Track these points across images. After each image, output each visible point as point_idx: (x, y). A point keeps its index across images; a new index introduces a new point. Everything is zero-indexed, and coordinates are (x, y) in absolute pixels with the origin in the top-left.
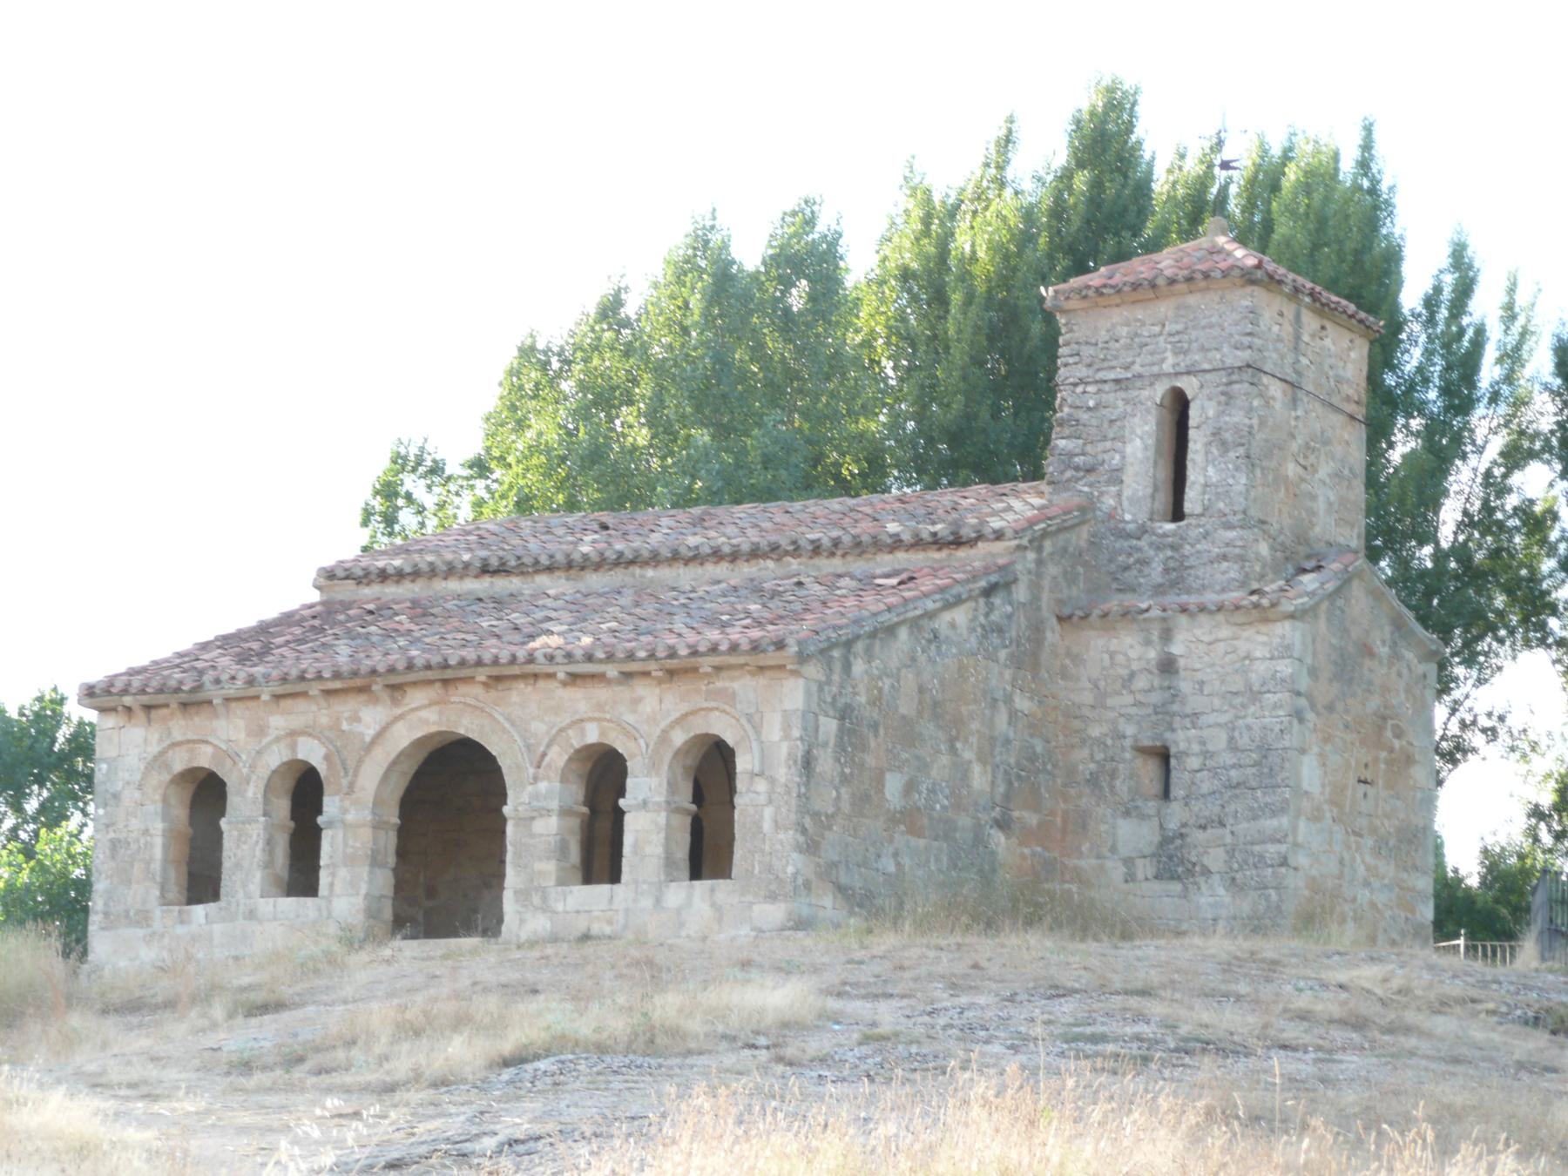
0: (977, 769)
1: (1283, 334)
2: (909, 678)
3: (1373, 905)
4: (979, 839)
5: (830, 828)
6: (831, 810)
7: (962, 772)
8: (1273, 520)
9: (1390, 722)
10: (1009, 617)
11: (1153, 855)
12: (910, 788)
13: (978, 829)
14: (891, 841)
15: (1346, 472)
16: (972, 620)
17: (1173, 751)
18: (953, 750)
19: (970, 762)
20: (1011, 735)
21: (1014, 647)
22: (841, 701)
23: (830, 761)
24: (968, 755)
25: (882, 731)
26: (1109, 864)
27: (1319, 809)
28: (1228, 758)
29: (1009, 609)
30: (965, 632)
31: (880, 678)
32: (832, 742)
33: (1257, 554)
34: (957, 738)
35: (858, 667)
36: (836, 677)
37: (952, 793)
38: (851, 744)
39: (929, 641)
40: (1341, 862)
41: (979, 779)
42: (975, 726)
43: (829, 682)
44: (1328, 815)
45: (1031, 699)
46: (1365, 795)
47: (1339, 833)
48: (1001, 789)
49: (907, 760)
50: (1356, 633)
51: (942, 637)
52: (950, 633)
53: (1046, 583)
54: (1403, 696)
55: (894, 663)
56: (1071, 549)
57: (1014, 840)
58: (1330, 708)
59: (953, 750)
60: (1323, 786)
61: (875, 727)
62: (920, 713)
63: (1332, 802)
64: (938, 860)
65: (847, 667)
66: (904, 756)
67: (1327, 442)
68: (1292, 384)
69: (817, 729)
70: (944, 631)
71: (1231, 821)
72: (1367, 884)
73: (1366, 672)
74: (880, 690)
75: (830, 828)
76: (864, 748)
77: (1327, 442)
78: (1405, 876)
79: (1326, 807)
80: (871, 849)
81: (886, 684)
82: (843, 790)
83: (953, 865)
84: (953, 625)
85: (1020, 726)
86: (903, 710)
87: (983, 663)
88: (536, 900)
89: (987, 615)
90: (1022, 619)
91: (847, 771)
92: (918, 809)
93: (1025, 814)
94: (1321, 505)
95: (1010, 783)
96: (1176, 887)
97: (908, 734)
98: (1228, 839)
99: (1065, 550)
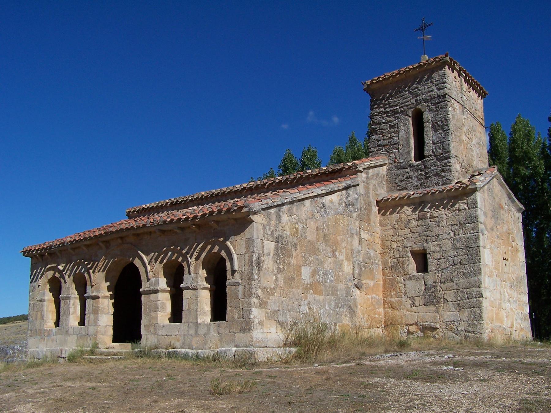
0: (346, 263)
1: (457, 85)
2: (312, 224)
4: (348, 293)
5: (273, 294)
6: (273, 286)
7: (339, 265)
8: (460, 156)
10: (357, 199)
12: (314, 273)
13: (348, 289)
14: (306, 298)
15: (481, 143)
16: (340, 200)
17: (428, 251)
18: (334, 255)
19: (343, 261)
20: (360, 249)
21: (359, 212)
22: (276, 234)
23: (271, 262)
24: (341, 257)
25: (298, 248)
26: (404, 300)
27: (492, 272)
28: (453, 253)
29: (356, 196)
30: (337, 205)
31: (297, 223)
32: (272, 254)
33: (456, 169)
34: (336, 250)
35: (285, 218)
36: (273, 222)
37: (335, 275)
38: (282, 254)
39: (321, 208)
41: (347, 268)
42: (344, 245)
43: (269, 225)
44: (495, 274)
45: (368, 234)
48: (357, 272)
49: (312, 261)
51: (327, 207)
52: (330, 205)
53: (371, 187)
55: (304, 216)
56: (380, 175)
57: (364, 292)
58: (492, 229)
59: (334, 255)
61: (295, 246)
62: (318, 240)
63: (496, 269)
64: (330, 305)
65: (279, 218)
66: (311, 259)
67: (474, 131)
69: (263, 247)
70: (327, 204)
71: (456, 279)
73: (502, 216)
74: (297, 229)
75: (273, 294)
76: (290, 256)
77: (474, 131)
78: (520, 296)
79: (494, 271)
80: (296, 303)
81: (300, 226)
82: (279, 276)
83: (337, 306)
84: (332, 202)
85: (363, 245)
86: (309, 238)
87: (346, 218)
88: (152, 330)
89: (347, 198)
90: (362, 201)
91: (281, 267)
92: (319, 282)
93: (368, 281)
94: (475, 154)
95: (361, 269)
96: (433, 308)
97: (312, 249)
98: (455, 287)
99: (378, 174)
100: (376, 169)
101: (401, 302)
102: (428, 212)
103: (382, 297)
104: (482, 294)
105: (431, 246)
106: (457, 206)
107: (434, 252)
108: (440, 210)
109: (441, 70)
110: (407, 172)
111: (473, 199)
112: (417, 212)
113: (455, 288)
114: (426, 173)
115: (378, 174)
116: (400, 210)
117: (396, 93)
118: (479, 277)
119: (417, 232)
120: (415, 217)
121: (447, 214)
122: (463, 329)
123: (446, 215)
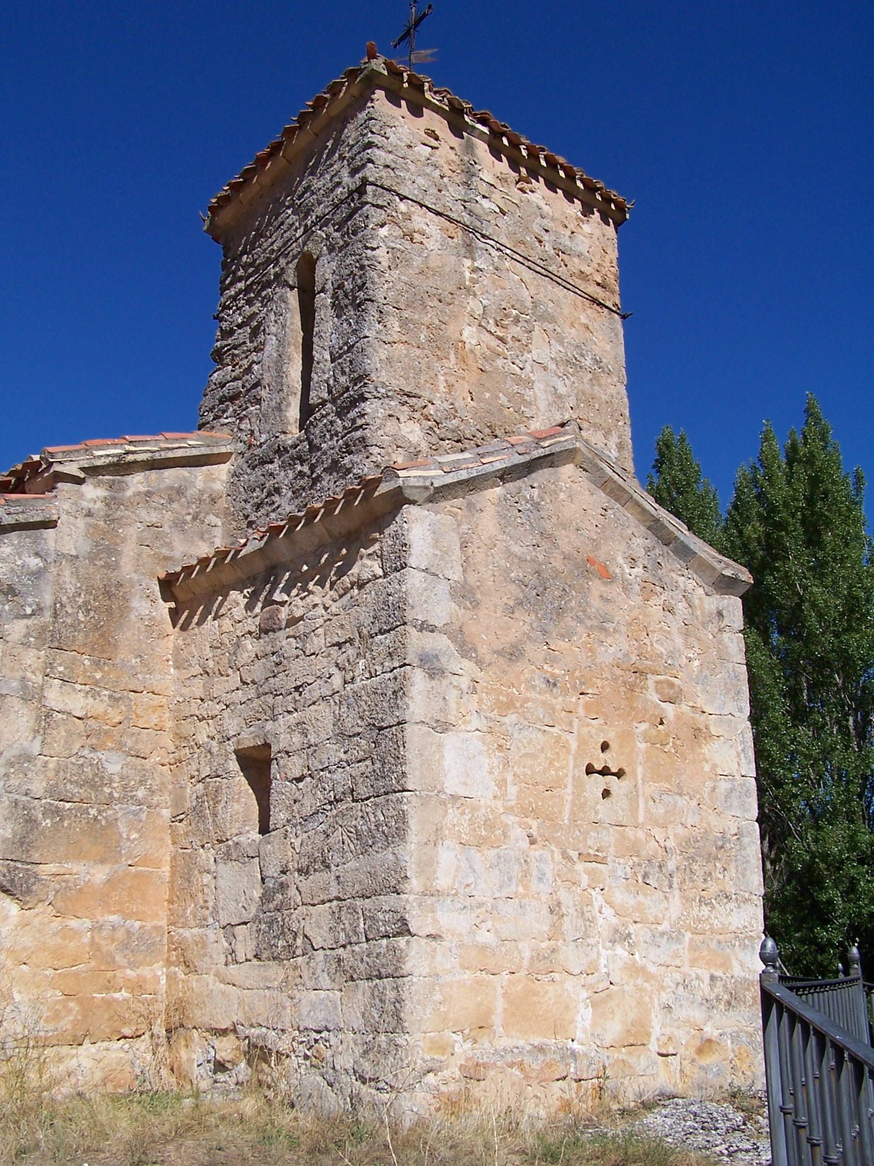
3: (636, 970)
9: (652, 680)
10: (38, 574)
11: (256, 919)
20: (36, 748)
21: (47, 617)
40: (555, 909)
46: (606, 793)
47: (547, 860)
50: (566, 541)
54: (679, 641)
56: (191, 492)
60: (502, 784)
68: (466, 228)
72: (620, 937)
73: (595, 602)
100: (168, 473)
101: (202, 942)
102: (283, 604)
103: (163, 923)
104: (403, 921)
105: (282, 733)
106: (355, 570)
107: (287, 753)
108: (311, 592)
109: (362, 108)
110: (271, 474)
111: (396, 536)
112: (257, 610)
113: (335, 894)
114: (312, 468)
115: (180, 492)
116: (221, 605)
117: (270, 223)
118: (399, 850)
119: (253, 682)
120: (252, 625)
121: (329, 602)
122: (349, 1066)
123: (326, 608)
